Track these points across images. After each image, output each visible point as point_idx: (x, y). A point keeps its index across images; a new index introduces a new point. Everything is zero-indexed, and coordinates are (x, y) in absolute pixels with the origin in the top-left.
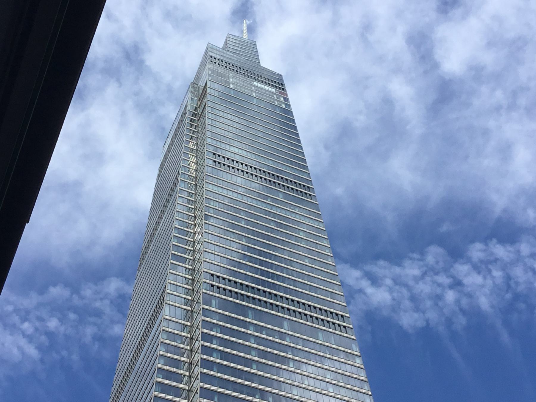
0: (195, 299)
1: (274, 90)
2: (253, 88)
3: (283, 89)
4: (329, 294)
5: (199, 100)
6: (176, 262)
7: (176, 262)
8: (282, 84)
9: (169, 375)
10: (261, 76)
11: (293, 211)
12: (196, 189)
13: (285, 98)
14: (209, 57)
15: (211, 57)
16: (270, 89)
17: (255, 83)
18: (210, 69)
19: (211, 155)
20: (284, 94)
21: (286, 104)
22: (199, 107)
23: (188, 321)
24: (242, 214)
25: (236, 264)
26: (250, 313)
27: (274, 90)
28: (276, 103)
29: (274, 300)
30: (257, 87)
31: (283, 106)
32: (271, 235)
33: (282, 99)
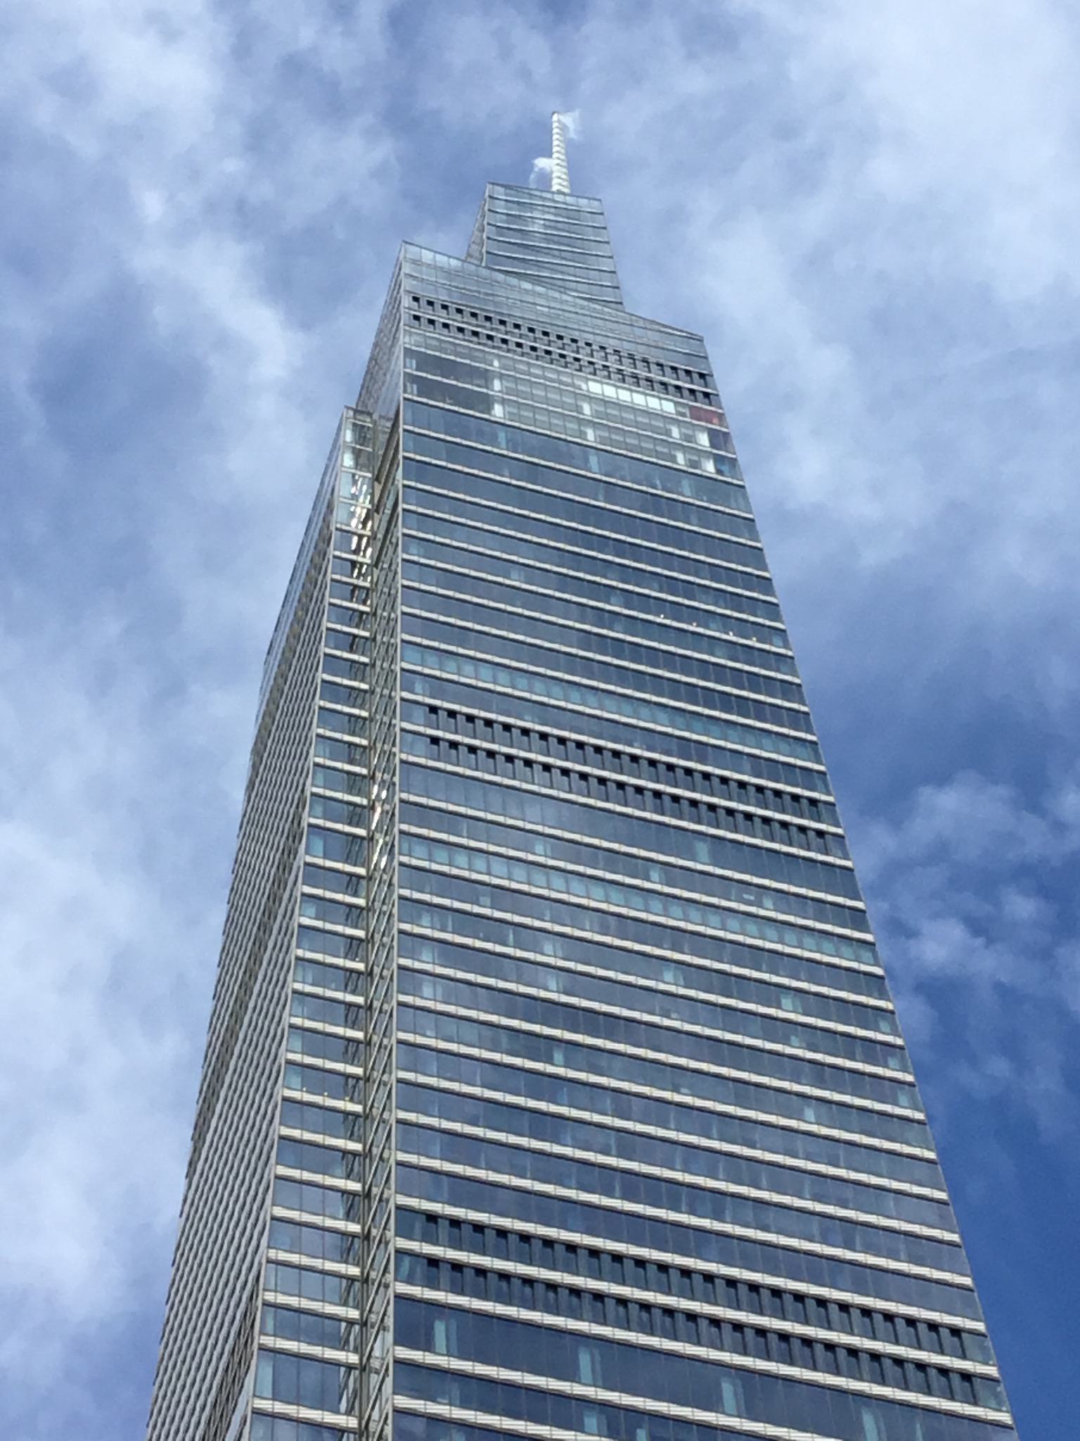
0: (373, 1275)
1: (669, 407)
2: (587, 409)
3: (707, 395)
4: (841, 1151)
5: (377, 479)
6: (295, 1173)
7: (295, 1173)
8: (702, 376)
9: (353, 643)
10: (631, 357)
11: (753, 909)
12: (364, 1296)
13: (713, 435)
14: (407, 301)
15: (416, 299)
16: (654, 403)
17: (594, 388)
18: (408, 352)
19: (420, 713)
20: (708, 416)
21: (718, 460)
22: (377, 511)
23: (349, 1412)
24: (548, 948)
25: (504, 1038)
26: (584, 1360)
27: (669, 407)
28: (680, 458)
29: (681, 1295)
30: (605, 402)
31: (709, 467)
32: (666, 1022)
33: (704, 440)
